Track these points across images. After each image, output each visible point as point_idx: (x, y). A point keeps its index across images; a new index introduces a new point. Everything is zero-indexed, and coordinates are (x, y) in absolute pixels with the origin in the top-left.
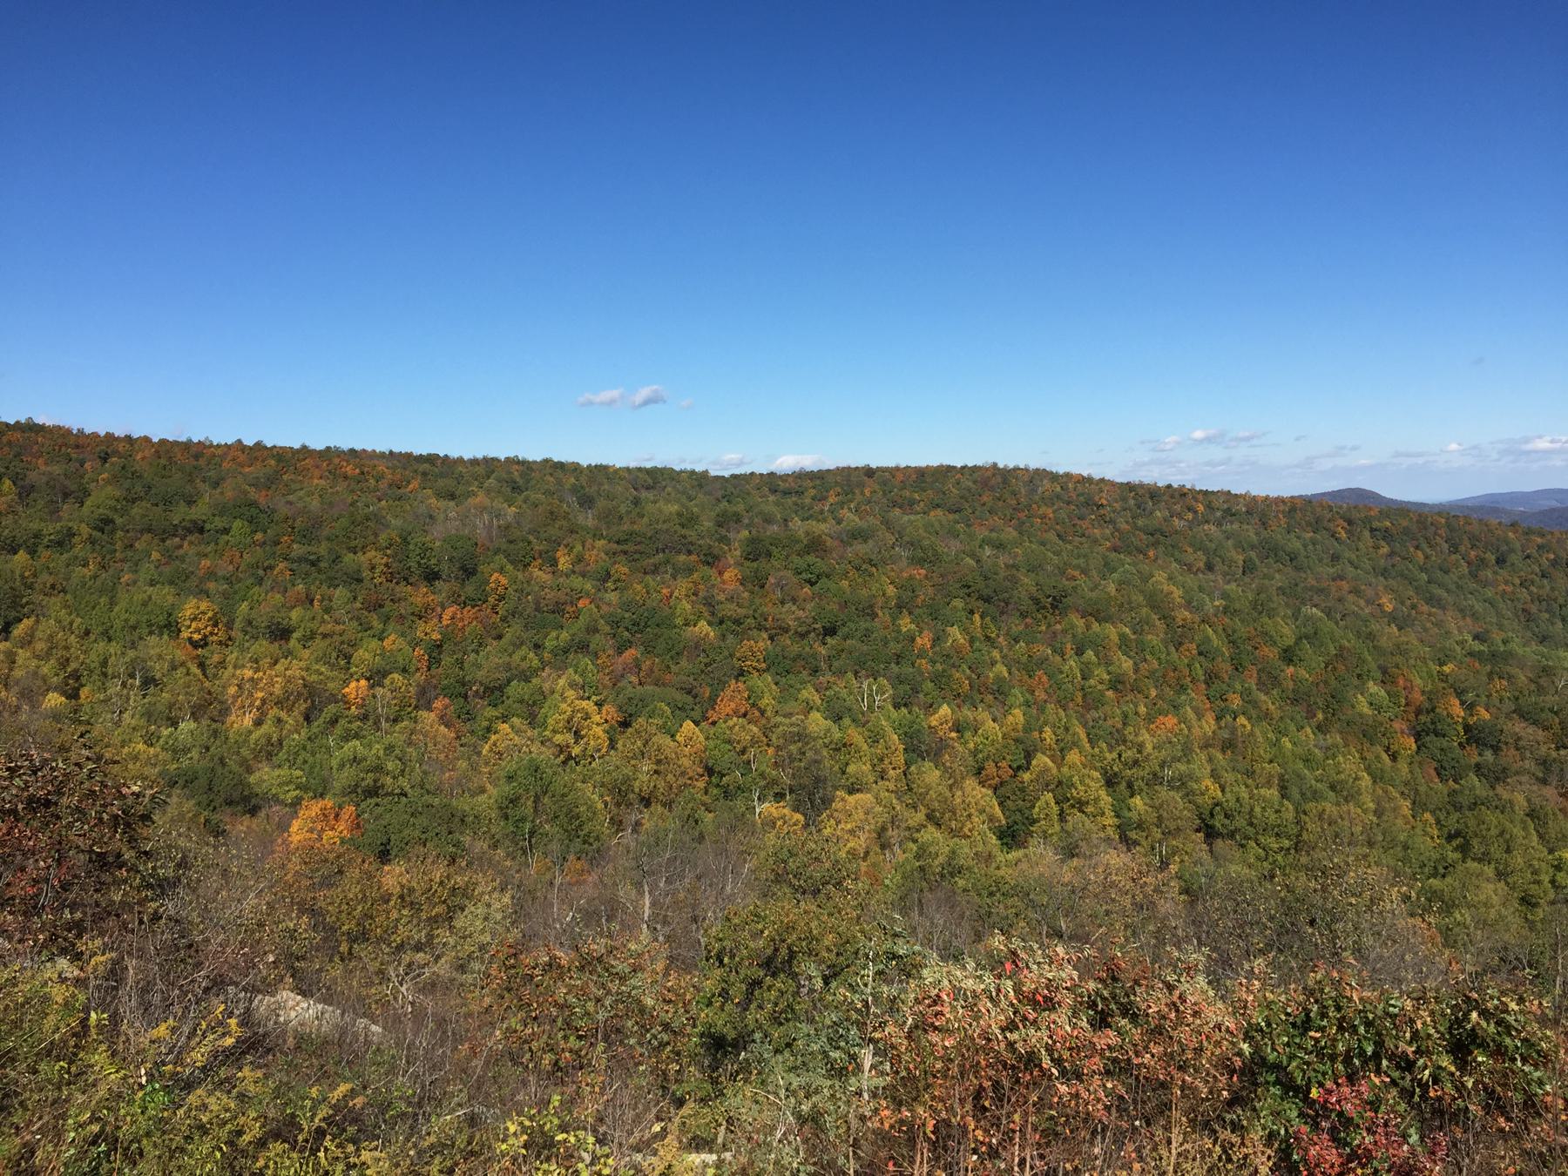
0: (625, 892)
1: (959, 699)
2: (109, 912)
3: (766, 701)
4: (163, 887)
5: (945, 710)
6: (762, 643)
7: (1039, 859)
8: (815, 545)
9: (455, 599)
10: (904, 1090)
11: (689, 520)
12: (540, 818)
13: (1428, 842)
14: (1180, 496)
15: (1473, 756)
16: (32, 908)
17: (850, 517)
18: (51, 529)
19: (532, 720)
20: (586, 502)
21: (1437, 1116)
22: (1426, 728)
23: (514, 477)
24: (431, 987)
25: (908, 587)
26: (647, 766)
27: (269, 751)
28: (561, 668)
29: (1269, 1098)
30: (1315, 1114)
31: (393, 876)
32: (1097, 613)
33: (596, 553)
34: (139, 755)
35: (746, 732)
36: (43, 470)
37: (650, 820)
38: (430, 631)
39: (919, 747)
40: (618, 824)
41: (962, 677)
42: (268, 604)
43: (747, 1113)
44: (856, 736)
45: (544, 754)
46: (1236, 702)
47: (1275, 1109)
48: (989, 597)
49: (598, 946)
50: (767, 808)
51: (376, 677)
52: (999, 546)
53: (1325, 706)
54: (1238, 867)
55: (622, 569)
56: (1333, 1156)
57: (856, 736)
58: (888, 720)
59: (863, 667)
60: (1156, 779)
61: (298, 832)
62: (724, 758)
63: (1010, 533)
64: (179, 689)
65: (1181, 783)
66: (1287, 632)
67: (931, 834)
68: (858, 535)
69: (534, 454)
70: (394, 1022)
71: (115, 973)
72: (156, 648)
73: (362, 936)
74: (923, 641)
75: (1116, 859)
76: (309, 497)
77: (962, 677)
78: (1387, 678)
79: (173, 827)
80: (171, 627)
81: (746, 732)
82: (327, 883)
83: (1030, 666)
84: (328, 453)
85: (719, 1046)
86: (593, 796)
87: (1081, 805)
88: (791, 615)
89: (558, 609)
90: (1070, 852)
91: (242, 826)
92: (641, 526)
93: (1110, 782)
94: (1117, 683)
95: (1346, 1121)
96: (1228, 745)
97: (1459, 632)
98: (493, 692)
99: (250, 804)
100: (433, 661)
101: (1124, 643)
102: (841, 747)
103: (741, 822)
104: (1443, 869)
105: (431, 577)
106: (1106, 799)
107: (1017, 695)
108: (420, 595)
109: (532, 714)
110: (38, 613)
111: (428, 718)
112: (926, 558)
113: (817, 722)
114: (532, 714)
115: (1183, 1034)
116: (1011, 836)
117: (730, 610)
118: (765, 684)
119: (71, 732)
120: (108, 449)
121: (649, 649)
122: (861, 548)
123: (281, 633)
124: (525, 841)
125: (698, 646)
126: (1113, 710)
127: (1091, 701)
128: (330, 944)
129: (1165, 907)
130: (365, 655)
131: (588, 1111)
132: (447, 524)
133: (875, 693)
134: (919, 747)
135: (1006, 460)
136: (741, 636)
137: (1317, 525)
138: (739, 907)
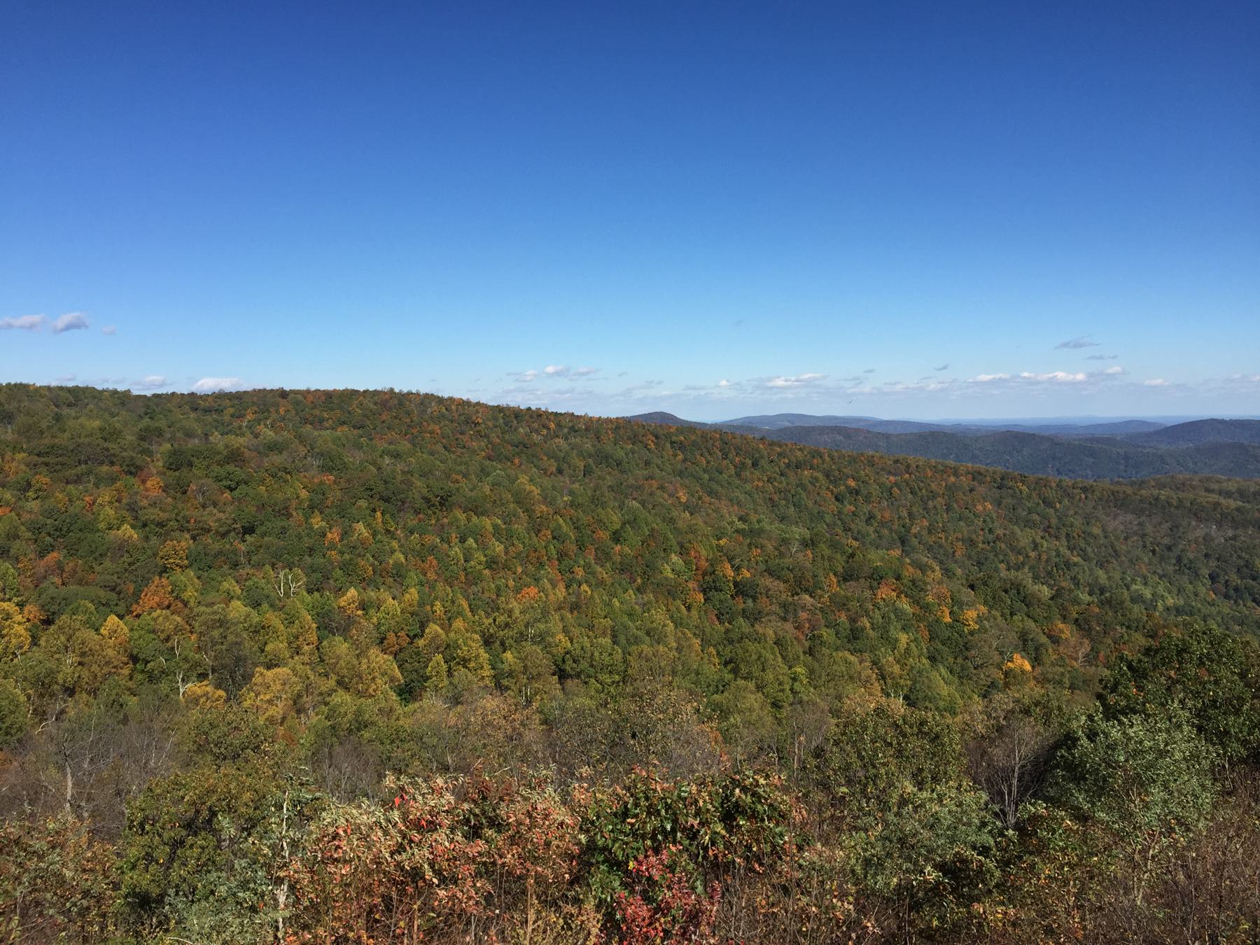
3: (190, 594)
5: (352, 592)
6: (185, 542)
7: (432, 707)
8: (234, 457)
11: (110, 435)
13: (712, 670)
15: (740, 604)
17: (268, 434)
21: (717, 868)
25: (319, 491)
26: (71, 659)
29: (599, 874)
32: (475, 509)
35: (169, 621)
39: (329, 624)
40: (41, 714)
44: (274, 619)
46: (580, 573)
48: (389, 498)
52: (397, 456)
53: (641, 573)
54: (583, 700)
55: (43, 479)
56: (644, 912)
57: (274, 619)
58: (303, 604)
59: (278, 559)
60: (522, 636)
63: (405, 446)
65: (541, 639)
67: (342, 698)
68: (273, 447)
74: (333, 535)
75: (491, 703)
77: (366, 564)
78: (683, 551)
81: (169, 621)
83: (423, 553)
85: (144, 903)
87: (464, 662)
88: (213, 517)
90: (456, 701)
92: (63, 439)
93: (487, 642)
94: (492, 564)
96: (575, 607)
102: (259, 630)
104: (722, 687)
107: (413, 577)
112: (331, 464)
113: (238, 609)
117: (153, 514)
118: (188, 581)
121: (72, 552)
122: (277, 459)
125: (123, 547)
127: (473, 579)
129: (529, 736)
133: (290, 583)
134: (329, 624)
135: (401, 386)
136: (164, 537)
137: (634, 439)
138: (165, 777)
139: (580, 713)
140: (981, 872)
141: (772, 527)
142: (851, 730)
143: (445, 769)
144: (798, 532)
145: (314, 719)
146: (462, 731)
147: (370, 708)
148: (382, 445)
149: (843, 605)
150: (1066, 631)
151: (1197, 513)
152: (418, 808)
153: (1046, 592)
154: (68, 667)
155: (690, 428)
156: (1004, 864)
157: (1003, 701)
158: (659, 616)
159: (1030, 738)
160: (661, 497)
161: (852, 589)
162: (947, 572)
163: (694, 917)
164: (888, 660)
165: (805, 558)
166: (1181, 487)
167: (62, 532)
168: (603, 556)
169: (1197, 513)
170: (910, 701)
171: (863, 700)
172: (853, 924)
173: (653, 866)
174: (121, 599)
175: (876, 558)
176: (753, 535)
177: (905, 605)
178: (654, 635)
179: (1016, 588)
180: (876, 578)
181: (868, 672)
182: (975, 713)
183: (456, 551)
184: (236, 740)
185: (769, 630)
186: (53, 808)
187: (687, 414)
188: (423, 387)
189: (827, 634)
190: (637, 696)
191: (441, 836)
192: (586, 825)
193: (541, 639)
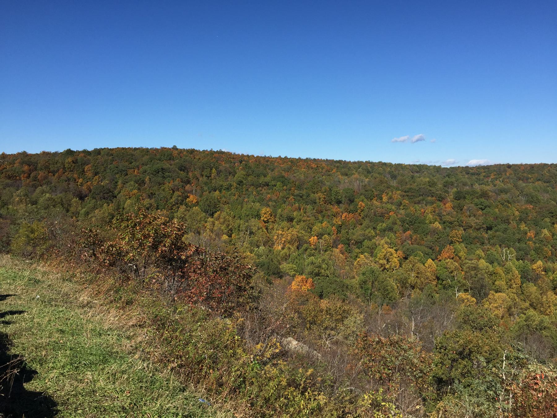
0: (405, 319)
1: (546, 258)
5: (540, 263)
6: (461, 232)
8: (484, 195)
9: (346, 210)
11: (432, 184)
16: (219, 302)
18: (225, 184)
19: (372, 254)
20: (394, 177)
23: (368, 168)
26: (413, 274)
27: (286, 258)
28: (383, 236)
31: (324, 304)
33: (397, 196)
34: (250, 257)
35: (453, 265)
36: (224, 166)
38: (338, 221)
40: (402, 295)
42: (286, 210)
44: (500, 270)
51: (320, 236)
55: (406, 202)
57: (500, 270)
58: (513, 265)
59: (503, 243)
61: (294, 285)
62: (444, 274)
64: (260, 236)
67: (531, 312)
68: (502, 191)
69: (375, 160)
72: (253, 222)
73: (313, 323)
76: (300, 175)
80: (258, 216)
81: (453, 265)
82: (303, 303)
85: (440, 382)
88: (473, 221)
89: (382, 215)
91: (277, 282)
92: (414, 186)
98: (359, 243)
99: (280, 275)
100: (339, 231)
103: (450, 299)
105: (339, 202)
108: (335, 209)
109: (372, 251)
110: (222, 210)
111: (337, 251)
112: (532, 200)
113: (483, 263)
114: (372, 251)
117: (448, 218)
118: (462, 248)
120: (243, 159)
121: (416, 231)
122: (504, 196)
123: (290, 220)
124: (369, 297)
125: (435, 231)
130: (317, 228)
132: (345, 184)
133: (509, 255)
134: (526, 276)
136: (452, 228)
138: (449, 331)
145: (519, 319)
174: (434, 253)
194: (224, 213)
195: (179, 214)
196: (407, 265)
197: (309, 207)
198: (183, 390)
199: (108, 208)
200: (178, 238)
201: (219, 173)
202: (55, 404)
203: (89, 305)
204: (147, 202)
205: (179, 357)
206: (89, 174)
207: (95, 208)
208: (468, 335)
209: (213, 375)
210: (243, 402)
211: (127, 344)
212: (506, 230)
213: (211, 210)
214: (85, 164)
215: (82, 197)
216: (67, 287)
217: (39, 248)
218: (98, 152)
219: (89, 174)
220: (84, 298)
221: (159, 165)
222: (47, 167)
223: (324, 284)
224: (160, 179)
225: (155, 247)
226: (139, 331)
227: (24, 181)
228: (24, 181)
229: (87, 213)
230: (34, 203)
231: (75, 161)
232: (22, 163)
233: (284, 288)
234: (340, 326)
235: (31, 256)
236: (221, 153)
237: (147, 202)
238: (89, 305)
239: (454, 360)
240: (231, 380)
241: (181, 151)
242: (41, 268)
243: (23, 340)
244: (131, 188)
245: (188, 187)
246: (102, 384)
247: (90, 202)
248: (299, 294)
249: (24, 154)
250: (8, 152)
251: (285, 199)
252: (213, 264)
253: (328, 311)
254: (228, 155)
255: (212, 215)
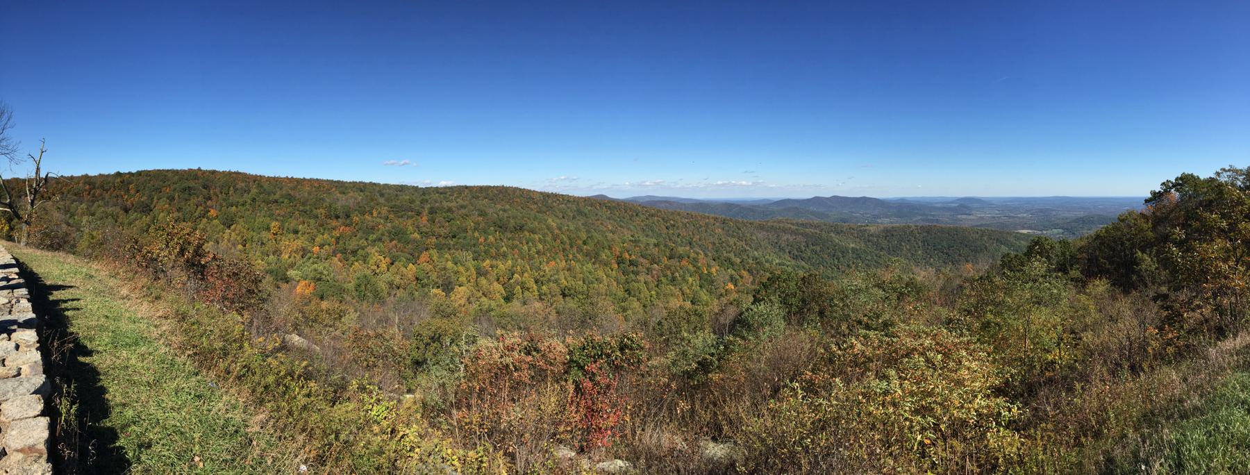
0: (391, 315)
1: (492, 257)
2: (250, 305)
3: (435, 258)
4: (264, 301)
5: (488, 261)
6: (434, 240)
7: (516, 305)
8: (450, 210)
9: (344, 224)
10: (472, 376)
11: (412, 201)
12: (366, 291)
13: (621, 294)
14: (556, 195)
15: (632, 268)
16: (233, 302)
17: (461, 202)
18: (241, 201)
19: (365, 261)
20: (382, 195)
21: (617, 368)
22: (620, 261)
23: (361, 187)
24: (334, 338)
25: (477, 223)
26: (398, 277)
27: (292, 266)
28: (373, 246)
29: (574, 371)
30: (586, 373)
31: (324, 305)
32: (532, 231)
33: (384, 210)
34: (260, 265)
35: (429, 267)
36: (241, 185)
37: (400, 293)
38: (336, 233)
39: (480, 273)
40: (389, 294)
41: (493, 251)
42: (293, 224)
43: (423, 383)
44: (461, 269)
45: (368, 272)
46: (571, 257)
47: (576, 374)
48: (501, 227)
49: (380, 331)
50: (435, 291)
51: (321, 246)
52: (505, 211)
53: (594, 257)
54: (571, 304)
55: (392, 216)
56: (590, 385)
57: (461, 269)
58: (471, 264)
59: (463, 248)
60: (549, 280)
61: (299, 289)
62: (421, 276)
63: (508, 207)
64: (270, 246)
65: (556, 281)
66: (584, 236)
67: (484, 299)
68: (463, 207)
69: (367, 181)
70: (323, 347)
71: (251, 322)
72: (264, 234)
73: (315, 321)
74: (481, 240)
75: (538, 305)
76: (305, 192)
77: (493, 251)
78: (610, 248)
79: (267, 284)
80: (268, 229)
81: (429, 267)
82: (306, 304)
83: (513, 247)
84: (311, 180)
85: (418, 363)
86: (382, 285)
87: (528, 289)
88: (442, 231)
89: (373, 228)
90: (525, 303)
91: (284, 286)
92: (398, 203)
93: (536, 282)
94: (538, 252)
95: (594, 374)
96: (569, 270)
97: (628, 236)
98: (354, 253)
99: (287, 280)
100: (337, 243)
101: (540, 240)
102: (456, 272)
103: (426, 295)
104: (624, 300)
105: (337, 217)
106: (535, 287)
107: (510, 257)
108: (334, 223)
109: (365, 260)
110: (237, 223)
111: (336, 259)
112: (482, 214)
113: (450, 265)
114: (365, 260)
115: (551, 355)
116: (508, 299)
117: (424, 229)
118: (434, 252)
119: (243, 256)
120: (257, 180)
121: (399, 241)
122: (464, 211)
123: (296, 232)
124: (362, 297)
125: (415, 241)
126: (536, 262)
127: (531, 258)
128: (306, 322)
129: (551, 318)
130: (319, 239)
131: (376, 380)
132: (342, 201)
133: (467, 256)
134: (480, 273)
135: (507, 184)
136: (427, 237)
137: (592, 205)
138: (426, 321)
139: (570, 310)
140: (711, 363)
141: (643, 239)
142: (671, 314)
143: (520, 328)
144: (654, 241)
145: (475, 306)
146: (527, 315)
147: (493, 304)
148: (499, 207)
149: (669, 268)
150: (745, 274)
151: (785, 230)
152: (508, 342)
153: (739, 260)
154: (397, 280)
155: (613, 201)
156: (719, 360)
157: (724, 300)
158: (601, 273)
159: (732, 312)
160: (601, 228)
161: (674, 262)
162: (706, 255)
163: (608, 387)
164: (685, 288)
165: (655, 251)
166: (779, 222)
167: (398, 234)
168: (580, 250)
169: (785, 230)
170: (693, 303)
171: (675, 303)
172: (668, 385)
173: (593, 367)
174: (414, 258)
175: (681, 250)
176: (636, 242)
177: (690, 267)
178: (599, 280)
179: (728, 260)
180: (681, 257)
181: (678, 293)
182: (715, 306)
183: (526, 247)
184: (449, 310)
185: (642, 278)
186: (392, 326)
187: (612, 195)
188: (515, 185)
189: (664, 280)
190: (592, 304)
191: (515, 354)
192: (570, 353)
193: (556, 281)
194: (240, 226)
195: (201, 226)
196: (392, 269)
197: (312, 221)
198: (197, 374)
199: (147, 219)
200: (200, 246)
201: (236, 190)
202: (99, 374)
203: (127, 297)
204: (176, 215)
205: (195, 347)
206: (132, 192)
207: (136, 219)
208: (438, 322)
209: (222, 365)
210: (246, 388)
211: (155, 333)
212: (465, 238)
213: (228, 223)
214: (130, 183)
215: (126, 211)
216: (112, 282)
217: (97, 250)
218: (139, 173)
219: (132, 192)
220: (124, 292)
221: (186, 184)
222: (102, 187)
223: (324, 287)
224: (186, 196)
225: (182, 252)
226: (164, 321)
227: (86, 198)
228: (86, 198)
229: (130, 224)
230: (93, 215)
231: (122, 181)
232: (85, 183)
233: (290, 292)
234: (337, 323)
235: (90, 256)
236: (237, 173)
237: (176, 215)
238: (127, 297)
239: (428, 344)
240: (237, 368)
241: (204, 172)
242: (95, 266)
243: (79, 321)
244: (164, 203)
245: (209, 203)
246: (133, 361)
247: (133, 215)
248: (302, 296)
249: (86, 176)
250: (76, 175)
251: (291, 215)
252: (228, 270)
253: (328, 311)
254: (245, 175)
255: (229, 227)
